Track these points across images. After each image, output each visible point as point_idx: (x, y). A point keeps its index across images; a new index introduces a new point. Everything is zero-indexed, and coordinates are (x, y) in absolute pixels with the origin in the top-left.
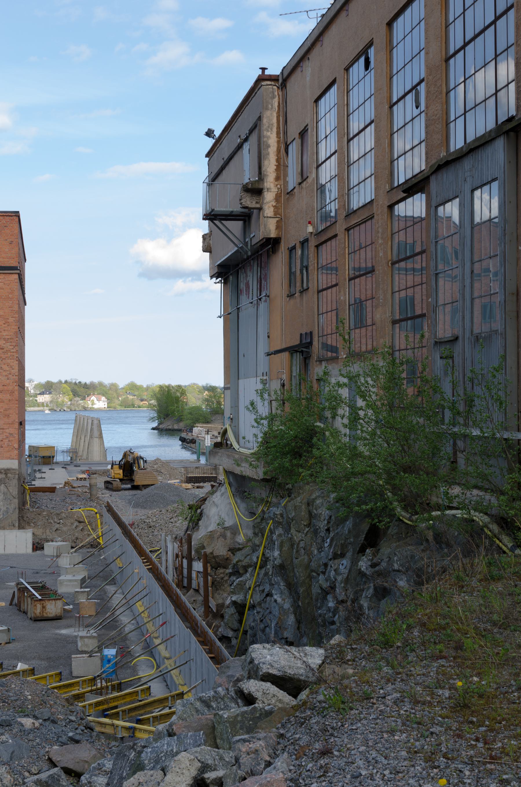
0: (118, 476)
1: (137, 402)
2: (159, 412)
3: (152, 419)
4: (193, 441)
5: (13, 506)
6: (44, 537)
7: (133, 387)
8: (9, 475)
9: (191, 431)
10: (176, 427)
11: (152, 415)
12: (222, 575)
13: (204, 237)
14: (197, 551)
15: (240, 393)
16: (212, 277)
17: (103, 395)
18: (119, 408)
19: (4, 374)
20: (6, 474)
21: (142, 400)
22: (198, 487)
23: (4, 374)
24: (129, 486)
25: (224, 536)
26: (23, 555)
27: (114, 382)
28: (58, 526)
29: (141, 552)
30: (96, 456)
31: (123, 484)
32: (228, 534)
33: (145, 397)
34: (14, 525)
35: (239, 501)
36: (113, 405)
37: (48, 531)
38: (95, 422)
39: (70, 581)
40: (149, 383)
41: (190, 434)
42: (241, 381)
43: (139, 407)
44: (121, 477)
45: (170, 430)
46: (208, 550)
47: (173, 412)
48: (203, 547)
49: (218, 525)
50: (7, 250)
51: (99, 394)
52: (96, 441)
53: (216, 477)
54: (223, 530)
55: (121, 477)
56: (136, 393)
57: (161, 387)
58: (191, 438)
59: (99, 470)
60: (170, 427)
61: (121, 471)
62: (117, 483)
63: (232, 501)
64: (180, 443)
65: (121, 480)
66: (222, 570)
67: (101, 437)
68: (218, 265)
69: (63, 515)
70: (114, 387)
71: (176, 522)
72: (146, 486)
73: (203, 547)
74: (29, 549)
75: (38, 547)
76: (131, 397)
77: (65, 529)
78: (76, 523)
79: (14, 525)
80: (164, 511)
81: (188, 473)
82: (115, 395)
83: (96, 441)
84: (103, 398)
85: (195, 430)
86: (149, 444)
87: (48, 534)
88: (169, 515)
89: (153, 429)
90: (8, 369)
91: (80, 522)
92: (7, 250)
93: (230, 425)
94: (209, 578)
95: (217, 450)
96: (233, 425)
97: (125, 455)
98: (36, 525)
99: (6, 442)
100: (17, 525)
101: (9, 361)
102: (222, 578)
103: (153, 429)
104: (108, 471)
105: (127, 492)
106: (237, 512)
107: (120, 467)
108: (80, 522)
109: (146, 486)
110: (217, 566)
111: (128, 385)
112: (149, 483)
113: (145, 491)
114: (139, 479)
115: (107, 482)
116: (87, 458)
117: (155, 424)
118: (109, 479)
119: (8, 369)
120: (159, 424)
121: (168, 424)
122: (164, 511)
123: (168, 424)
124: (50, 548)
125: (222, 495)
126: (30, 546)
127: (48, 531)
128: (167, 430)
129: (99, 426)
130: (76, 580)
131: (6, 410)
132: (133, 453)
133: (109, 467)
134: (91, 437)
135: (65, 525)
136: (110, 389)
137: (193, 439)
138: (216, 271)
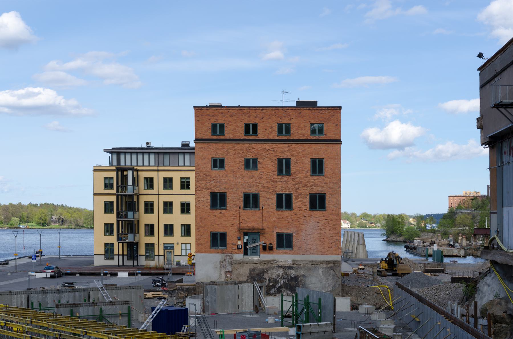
0: (384, 267)
1: (368, 225)
2: (387, 230)
3: (383, 235)
4: (415, 248)
5: (338, 283)
6: (356, 302)
7: (365, 216)
8: (336, 264)
9: (413, 242)
10: (398, 239)
11: (383, 232)
12: (499, 328)
13: (478, 120)
14: (481, 312)
15: (504, 215)
16: (482, 145)
17: (348, 220)
18: (357, 228)
19: (333, 204)
20: (334, 264)
21: (371, 223)
22: (434, 275)
23: (333, 204)
24: (391, 274)
25: (501, 304)
26: (345, 312)
27: (354, 212)
28: (365, 296)
29: (442, 313)
30: (361, 256)
31: (388, 272)
32: (503, 303)
33: (373, 222)
34: (339, 295)
35: (507, 282)
36: (353, 226)
37: (359, 298)
38: (361, 235)
39: (387, 328)
40: (375, 213)
41: (412, 244)
42: (505, 210)
43: (369, 227)
44: (387, 268)
45: (394, 241)
46: (490, 312)
47: (396, 231)
48: (487, 310)
49: (495, 296)
50: (334, 130)
51: (345, 219)
52: (361, 247)
53: (444, 270)
54: (499, 300)
55: (387, 268)
56: (368, 219)
57: (388, 215)
58: (413, 246)
59: (369, 264)
60: (395, 240)
61: (386, 265)
62: (384, 272)
63: (502, 282)
64: (405, 249)
65: (386, 270)
66: (499, 325)
67: (364, 244)
68: (489, 137)
69: (368, 289)
70: (353, 215)
71: (439, 295)
72: (404, 274)
73: (487, 310)
74: (349, 309)
75: (354, 307)
76: (364, 221)
77: (369, 297)
78: (376, 295)
79: (339, 295)
80: (430, 289)
81: (425, 266)
82: (354, 220)
83: (361, 247)
84: (347, 222)
85: (415, 241)
86: (383, 249)
87: (359, 300)
88: (434, 291)
89: (383, 240)
90: (335, 201)
91: (378, 294)
92: (334, 130)
93: (497, 236)
94: (492, 329)
95: (486, 251)
96: (499, 235)
97: (389, 255)
98: (351, 295)
99: (334, 244)
100: (341, 294)
101: (336, 196)
102: (499, 330)
103: (383, 240)
104: (378, 264)
105: (390, 277)
106: (506, 289)
107: (386, 262)
108: (378, 294)
109: (404, 274)
110: (496, 322)
111: (363, 214)
112: (406, 272)
113: (407, 276)
114: (400, 269)
115: (378, 271)
116: (356, 257)
117: (385, 238)
118: (379, 269)
119: (335, 201)
120: (388, 238)
121: (392, 238)
122: (430, 289)
123: (392, 238)
124: (363, 309)
125: (493, 278)
126: (349, 307)
127: (359, 298)
128: (392, 241)
129: (363, 238)
130: (391, 328)
131: (334, 225)
132: (395, 254)
133: (379, 262)
134: (358, 244)
135: (369, 295)
136: (352, 216)
137: (415, 247)
138: (488, 140)
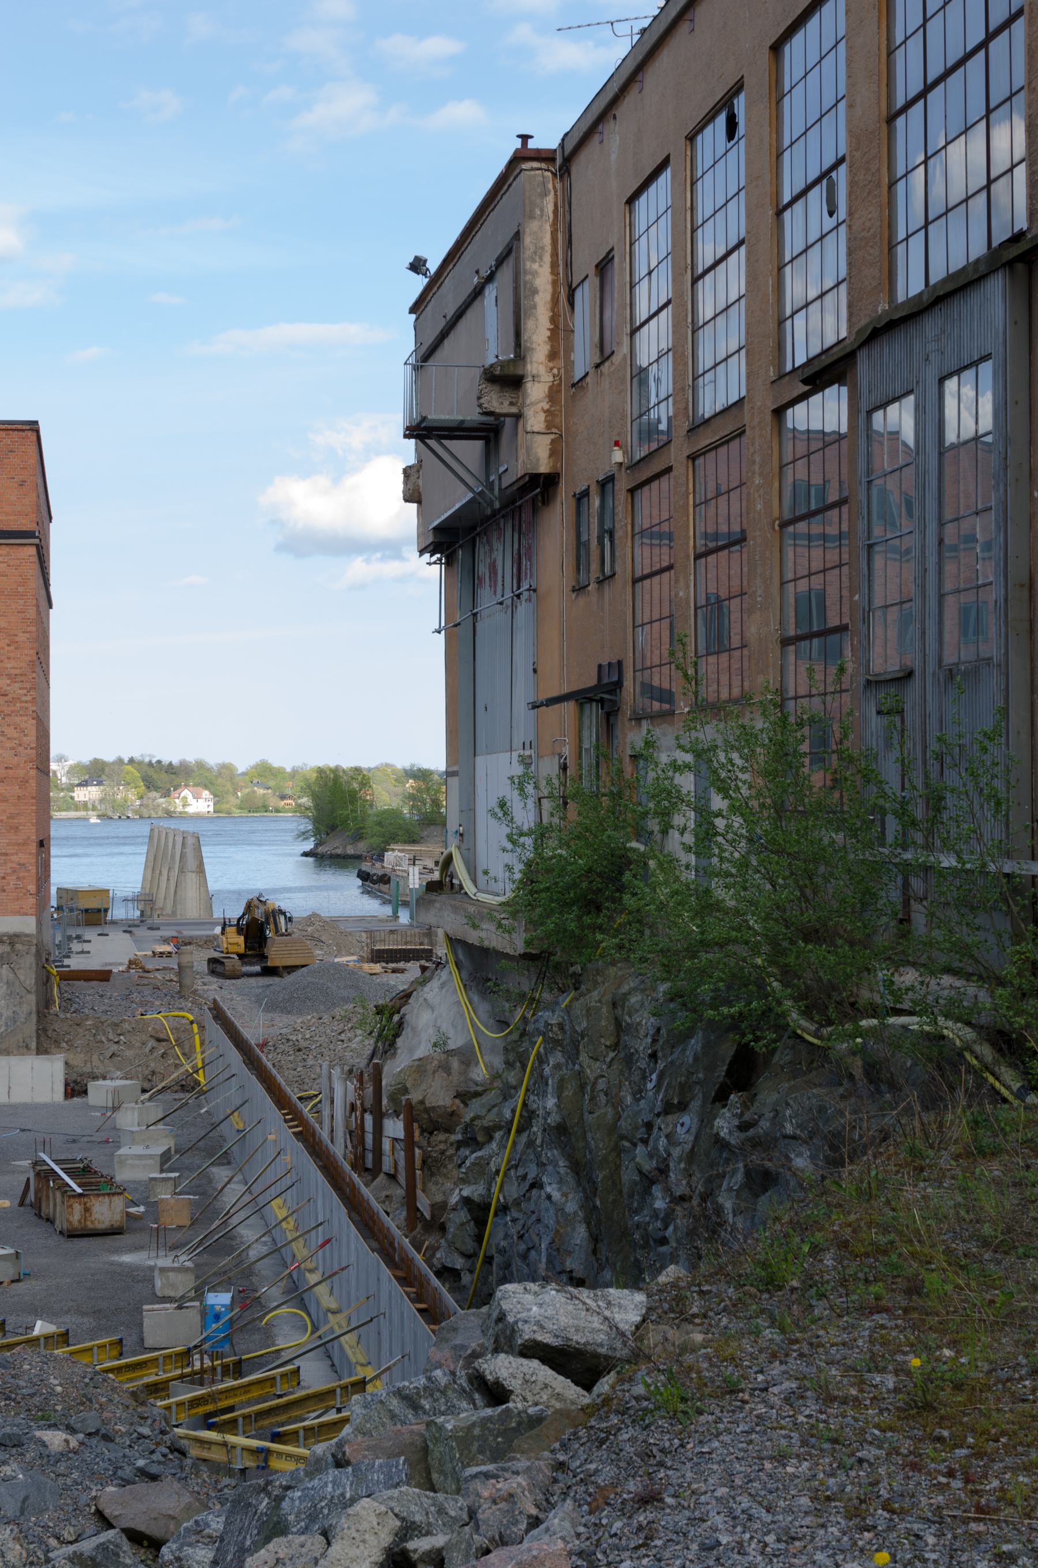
0: (235, 949)
1: (274, 802)
2: (316, 821)
3: (303, 835)
4: (385, 879)
5: (25, 1008)
6: (88, 1069)
7: (264, 772)
8: (18, 947)
9: (381, 858)
10: (350, 850)
11: (302, 828)
12: (442, 1147)
13: (407, 472)
14: (393, 1098)
15: (477, 782)
16: (422, 552)
17: (206, 787)
18: (237, 812)
19: (9, 744)
20: (12, 944)
21: (283, 797)
22: (394, 971)
23: (9, 744)
24: (257, 968)
25: (446, 1068)
26: (45, 1106)
27: (227, 761)
28: (115, 1047)
29: (281, 1100)
30: (192, 909)
31: (244, 964)
32: (455, 1064)
33: (289, 792)
34: (27, 1047)
35: (476, 998)
36: (224, 806)
37: (95, 1057)
38: (190, 841)
39: (140, 1157)
40: (298, 763)
41: (378, 865)
42: (479, 760)
43: (278, 811)
44: (241, 949)
45: (338, 856)
46: (415, 1096)
47: (344, 822)
48: (405, 1090)
49: (435, 1045)
50: (14, 498)
51: (196, 785)
52: (191, 879)
53: (431, 951)
54: (443, 1057)
55: (241, 949)
56: (272, 783)
57: (320, 771)
58: (380, 873)
59: (197, 937)
60: (339, 851)
61: (241, 939)
62: (233, 963)
63: (462, 998)
64: (359, 882)
65: (241, 956)
66: (442, 1137)
67: (201, 870)
68: (435, 529)
69: (126, 1026)
70: (226, 770)
71: (350, 1040)
72: (291, 969)
73: (405, 1090)
74: (59, 1094)
75: (75, 1089)
76: (261, 791)
77: (129, 1053)
78: (152, 1043)
79: (27, 1047)
80: (326, 1018)
81: (374, 942)
82: (229, 786)
83: (191, 879)
84: (206, 793)
85: (389, 856)
86: (297, 884)
87: (97, 1064)
88: (337, 1027)
89: (305, 854)
90: (16, 735)
91: (159, 1040)
92: (14, 498)
93: (459, 848)
94: (417, 1151)
95: (433, 896)
96: (464, 846)
97: (249, 907)
98: (71, 1047)
99: (12, 880)
100: (33, 1045)
101: (18, 719)
102: (443, 1152)
103: (305, 854)
104: (215, 937)
105: (252, 981)
106: (471, 1020)
107: (240, 931)
108: (159, 1040)
109: (291, 969)
110: (432, 1128)
111: (256, 767)
112: (298, 963)
113: (289, 979)
114: (277, 953)
115: (212, 961)
116: (174, 913)
117: (309, 846)
118: (216, 955)
119: (16, 735)
120: (316, 846)
121: (334, 845)
122: (326, 1018)
123: (334, 845)
124: (99, 1092)
125: (443, 986)
126: (60, 1089)
127: (95, 1057)
128: (332, 857)
129: (198, 849)
130: (151, 1157)
131: (11, 817)
132: (264, 903)
133: (218, 930)
134: (182, 870)
135: (129, 1045)
136: (220, 774)
137: (385, 875)
138: (430, 539)
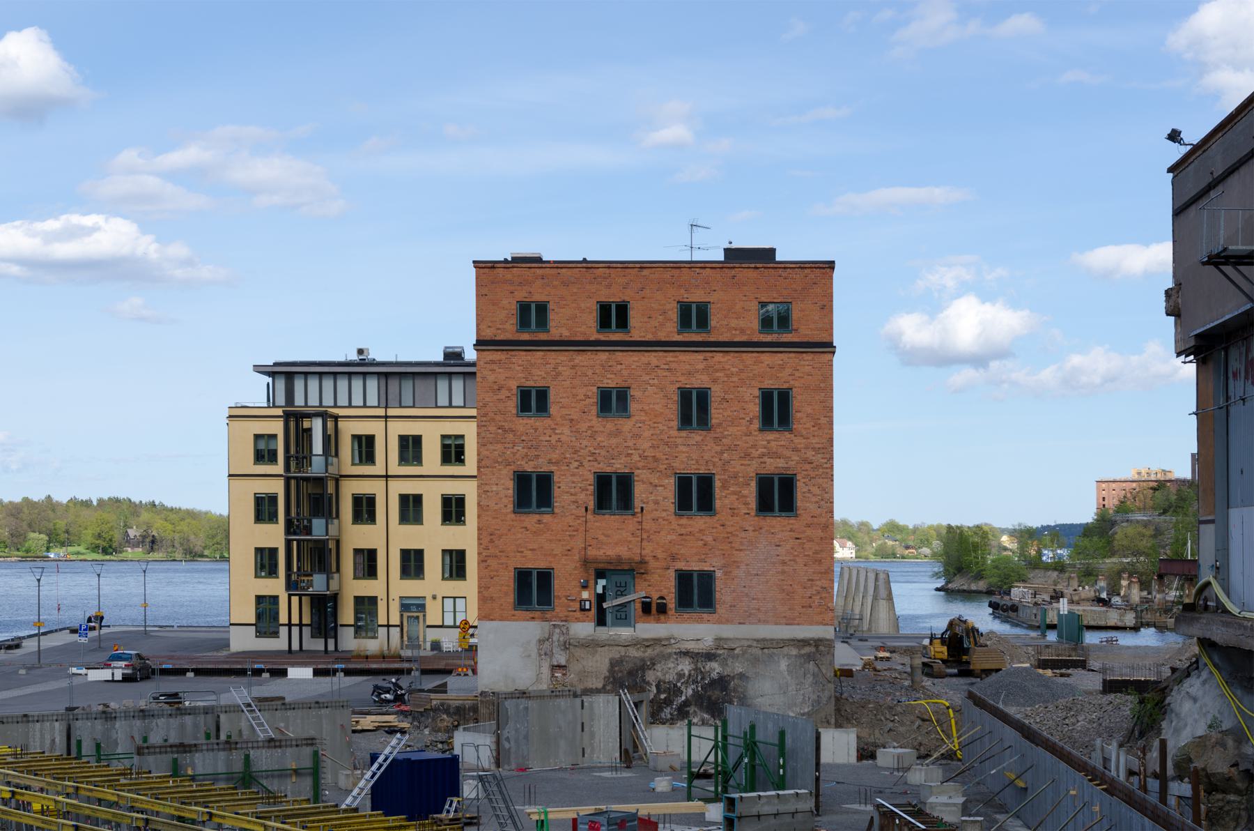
0: (940, 656)
1: (900, 551)
2: (947, 565)
3: (936, 575)
4: (1014, 608)
5: (827, 694)
6: (871, 740)
7: (893, 529)
8: (821, 648)
9: (1008, 593)
10: (973, 587)
11: (936, 569)
12: (1220, 804)
13: (1168, 293)
14: (1177, 765)
15: (1231, 528)
16: (1179, 354)
17: (850, 539)
18: (872, 558)
19: (814, 499)
20: (817, 646)
21: (907, 547)
22: (1062, 675)
23: (814, 499)
24: (956, 671)
25: (1224, 745)
26: (844, 766)
27: (865, 520)
28: (891, 725)
29: (1081, 767)
30: (883, 627)
31: (948, 667)
32: (1230, 743)
33: (911, 543)
34: (828, 722)
35: (1239, 692)
36: (863, 554)
37: (877, 731)
38: (882, 576)
39: (947, 805)
40: (918, 522)
41: (1007, 598)
42: (1234, 514)
43: (903, 557)
44: (945, 656)
45: (964, 591)
46: (1198, 764)
47: (969, 567)
48: (1190, 760)
49: (1210, 727)
50: (817, 318)
51: (842, 537)
52: (883, 604)
53: (1084, 661)
54: (1220, 736)
55: (945, 656)
56: (898, 537)
57: (949, 527)
58: (1009, 604)
59: (901, 647)
60: (965, 587)
61: (945, 649)
62: (938, 666)
63: (1226, 691)
64: (990, 610)
65: (944, 661)
66: (1220, 796)
67: (890, 598)
68: (1196, 336)
69: (899, 709)
70: (864, 526)
71: (1073, 724)
72: (987, 672)
73: (1190, 760)
74: (853, 759)
75: (866, 753)
76: (890, 543)
77: (901, 729)
78: (918, 722)
79: (828, 722)
80: (1051, 707)
81: (1040, 653)
82: (866, 539)
83: (883, 604)
84: (849, 544)
85: (1014, 591)
86: (936, 611)
87: (877, 736)
88: (1062, 714)
89: (937, 589)
90: (818, 492)
91: (924, 720)
92: (817, 318)
93: (1215, 578)
94: (1202, 806)
95: (1188, 615)
96: (1219, 577)
97: (951, 624)
98: (859, 724)
99: (816, 599)
100: (833, 721)
101: (820, 481)
102: (1221, 808)
103: (937, 589)
104: (925, 647)
105: (954, 680)
106: (1238, 708)
107: (943, 641)
108: (924, 720)
109: (987, 672)
110: (1212, 788)
111: (886, 525)
112: (993, 667)
113: (994, 677)
114: (978, 660)
115: (924, 664)
116: (869, 630)
117: (940, 583)
118: (926, 660)
119: (818, 492)
120: (947, 583)
121: (959, 583)
122: (1051, 707)
123: (959, 583)
124: (887, 756)
125: (1204, 683)
126: (854, 754)
127: (877, 731)
128: (959, 591)
129: (888, 582)
130: (955, 805)
131: (816, 552)
132: (965, 622)
133: (926, 642)
134: (875, 598)
135: (902, 723)
136: (860, 530)
137: (1013, 605)
138: (1192, 343)
